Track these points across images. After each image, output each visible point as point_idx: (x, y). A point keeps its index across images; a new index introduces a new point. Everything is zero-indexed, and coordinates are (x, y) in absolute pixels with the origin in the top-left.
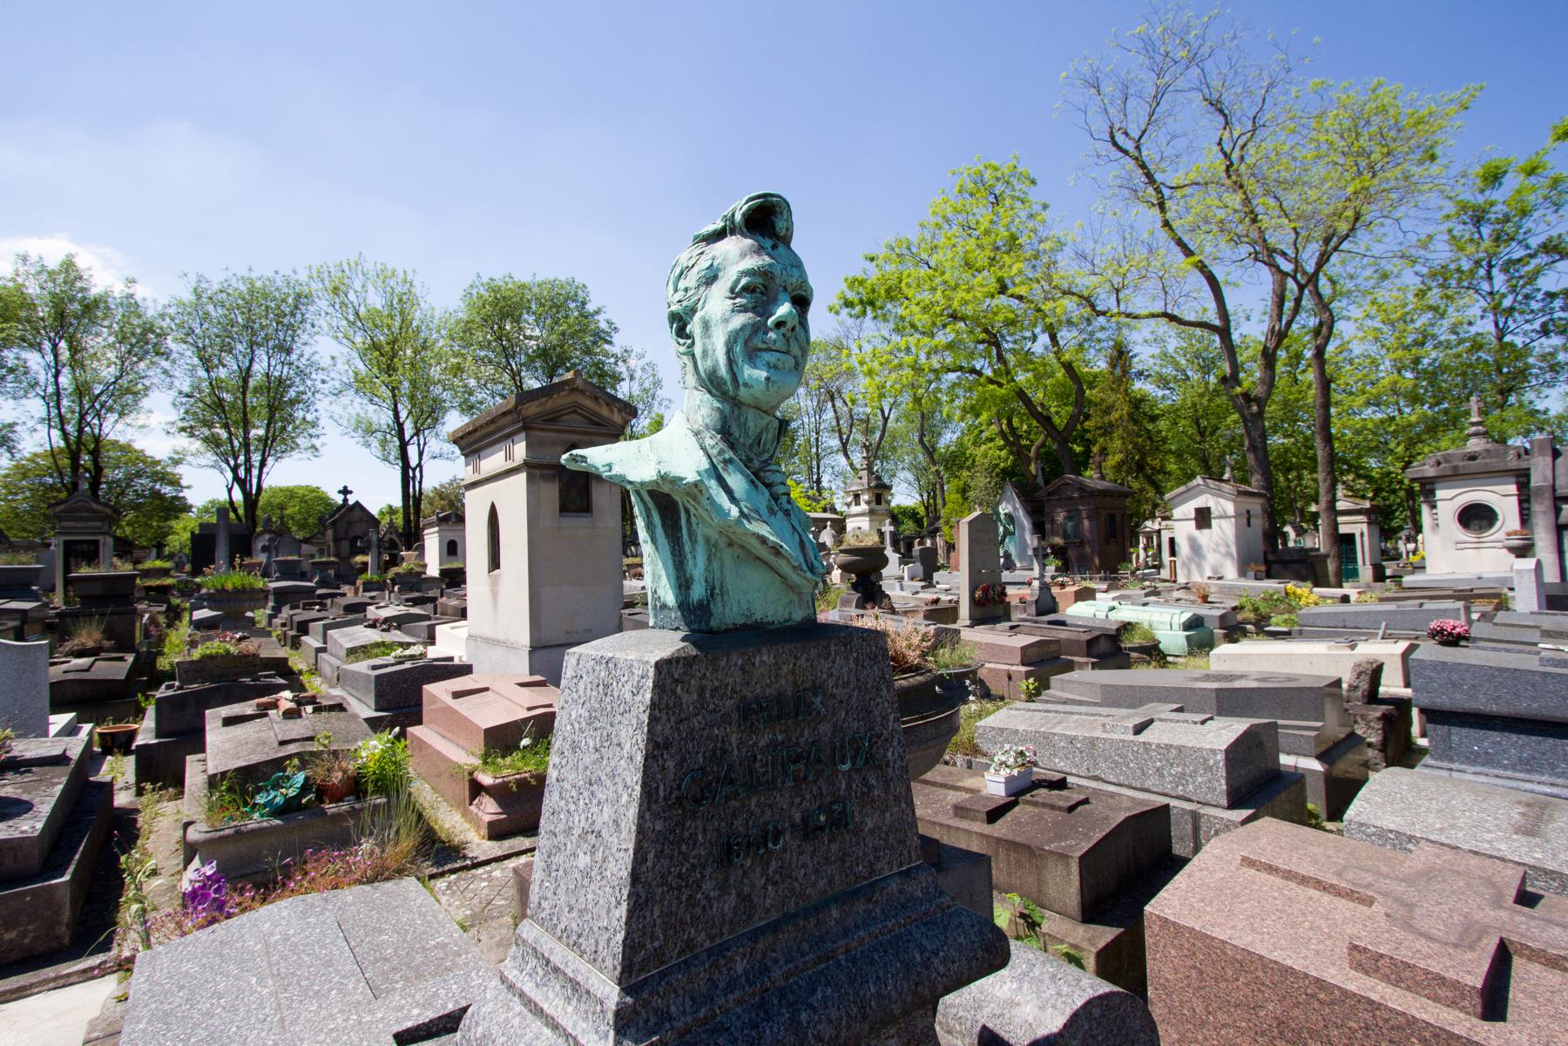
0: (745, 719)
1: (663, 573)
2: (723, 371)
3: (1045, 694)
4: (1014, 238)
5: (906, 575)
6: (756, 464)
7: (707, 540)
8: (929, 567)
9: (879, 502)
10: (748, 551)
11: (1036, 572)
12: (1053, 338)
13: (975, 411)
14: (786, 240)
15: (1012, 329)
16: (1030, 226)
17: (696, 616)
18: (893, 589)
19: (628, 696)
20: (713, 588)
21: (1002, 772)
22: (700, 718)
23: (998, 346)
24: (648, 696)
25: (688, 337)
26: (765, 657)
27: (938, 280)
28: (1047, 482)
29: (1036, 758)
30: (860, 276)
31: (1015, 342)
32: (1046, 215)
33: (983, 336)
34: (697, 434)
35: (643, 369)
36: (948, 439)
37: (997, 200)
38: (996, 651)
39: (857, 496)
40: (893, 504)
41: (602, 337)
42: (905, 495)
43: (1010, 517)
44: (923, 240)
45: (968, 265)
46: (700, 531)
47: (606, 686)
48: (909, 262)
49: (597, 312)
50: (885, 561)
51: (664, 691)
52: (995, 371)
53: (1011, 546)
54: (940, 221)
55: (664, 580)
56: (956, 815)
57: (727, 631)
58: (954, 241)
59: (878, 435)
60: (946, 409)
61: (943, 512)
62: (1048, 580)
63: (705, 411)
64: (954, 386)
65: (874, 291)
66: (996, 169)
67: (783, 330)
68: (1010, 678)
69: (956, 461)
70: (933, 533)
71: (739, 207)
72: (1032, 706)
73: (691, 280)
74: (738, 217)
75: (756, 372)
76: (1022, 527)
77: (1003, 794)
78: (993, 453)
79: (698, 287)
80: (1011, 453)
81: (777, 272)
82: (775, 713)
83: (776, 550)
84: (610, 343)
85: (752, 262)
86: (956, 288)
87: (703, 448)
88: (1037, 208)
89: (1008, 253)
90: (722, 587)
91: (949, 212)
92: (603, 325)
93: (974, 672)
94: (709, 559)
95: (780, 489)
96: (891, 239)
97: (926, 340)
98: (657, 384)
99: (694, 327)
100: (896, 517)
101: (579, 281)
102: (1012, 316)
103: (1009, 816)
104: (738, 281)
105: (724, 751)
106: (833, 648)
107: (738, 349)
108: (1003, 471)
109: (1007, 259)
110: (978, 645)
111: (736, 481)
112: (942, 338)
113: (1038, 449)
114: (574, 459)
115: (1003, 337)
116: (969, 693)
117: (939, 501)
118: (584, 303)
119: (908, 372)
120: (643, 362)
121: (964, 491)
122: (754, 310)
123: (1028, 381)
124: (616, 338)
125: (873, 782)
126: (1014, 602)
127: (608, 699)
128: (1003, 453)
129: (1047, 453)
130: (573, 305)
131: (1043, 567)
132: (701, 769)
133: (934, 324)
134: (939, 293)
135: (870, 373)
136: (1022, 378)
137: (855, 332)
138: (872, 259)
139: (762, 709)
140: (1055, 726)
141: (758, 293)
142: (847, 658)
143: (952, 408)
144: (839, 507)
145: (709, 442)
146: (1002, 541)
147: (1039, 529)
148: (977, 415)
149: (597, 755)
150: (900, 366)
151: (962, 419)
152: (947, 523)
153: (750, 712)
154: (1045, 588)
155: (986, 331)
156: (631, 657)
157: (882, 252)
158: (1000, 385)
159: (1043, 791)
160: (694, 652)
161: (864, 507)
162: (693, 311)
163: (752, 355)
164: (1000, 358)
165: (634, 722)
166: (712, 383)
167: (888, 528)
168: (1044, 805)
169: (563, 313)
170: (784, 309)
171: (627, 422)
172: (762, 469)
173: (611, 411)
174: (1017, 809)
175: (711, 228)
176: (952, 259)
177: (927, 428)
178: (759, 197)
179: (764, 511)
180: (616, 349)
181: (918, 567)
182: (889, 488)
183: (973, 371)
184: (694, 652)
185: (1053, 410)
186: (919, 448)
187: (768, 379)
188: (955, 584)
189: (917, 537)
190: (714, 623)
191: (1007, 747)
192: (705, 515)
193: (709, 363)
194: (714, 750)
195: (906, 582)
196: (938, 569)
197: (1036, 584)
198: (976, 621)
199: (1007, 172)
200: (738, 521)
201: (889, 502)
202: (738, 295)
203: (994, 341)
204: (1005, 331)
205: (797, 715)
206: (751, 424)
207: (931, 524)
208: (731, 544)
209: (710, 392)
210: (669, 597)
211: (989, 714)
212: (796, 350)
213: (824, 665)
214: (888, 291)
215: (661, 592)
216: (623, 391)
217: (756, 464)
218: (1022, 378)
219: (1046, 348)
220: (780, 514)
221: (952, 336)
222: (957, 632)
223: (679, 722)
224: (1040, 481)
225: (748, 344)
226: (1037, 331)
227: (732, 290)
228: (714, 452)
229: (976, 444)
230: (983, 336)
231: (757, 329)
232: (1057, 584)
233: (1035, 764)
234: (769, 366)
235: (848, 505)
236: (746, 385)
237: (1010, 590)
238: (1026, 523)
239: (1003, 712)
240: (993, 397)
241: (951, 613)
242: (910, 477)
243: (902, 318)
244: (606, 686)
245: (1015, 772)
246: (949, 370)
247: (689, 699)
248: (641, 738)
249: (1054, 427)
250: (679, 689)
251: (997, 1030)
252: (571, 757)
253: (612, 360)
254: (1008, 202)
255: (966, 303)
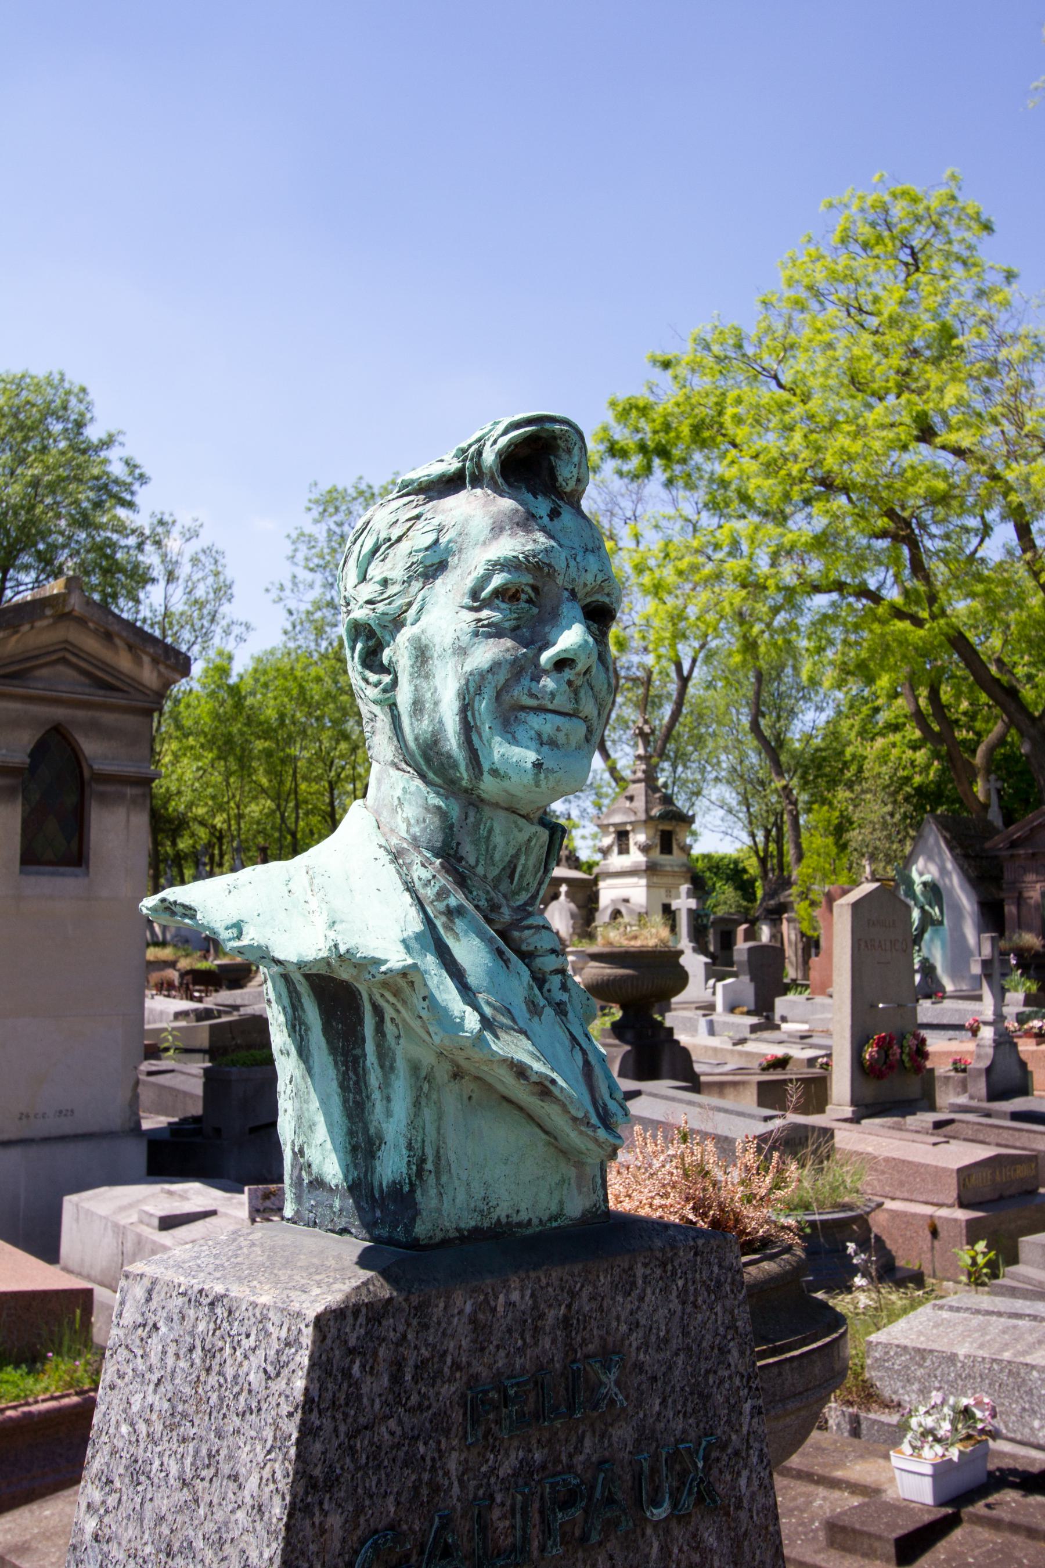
0: (475, 1422)
1: (320, 1119)
2: (452, 742)
3: (1010, 1274)
4: (947, 334)
5: (719, 1001)
6: (506, 915)
7: (415, 1068)
8: (767, 986)
9: (666, 847)
10: (488, 1087)
11: (987, 1008)
12: (1023, 531)
13: (865, 672)
14: (573, 500)
15: (941, 510)
16: (982, 312)
17: (383, 1211)
18: (693, 1030)
19: (255, 1378)
20: (423, 1160)
21: (927, 1452)
22: (392, 1423)
23: (914, 544)
24: (300, 1384)
25: (384, 669)
26: (515, 1295)
27: (798, 411)
28: (1009, 820)
29: (998, 1423)
30: (643, 396)
31: (947, 537)
32: (1008, 292)
33: (883, 523)
34: (396, 856)
35: (195, 561)
36: (808, 723)
37: (915, 263)
38: (907, 1176)
39: (622, 836)
40: (697, 850)
41: (113, 493)
42: (719, 834)
43: (934, 891)
44: (769, 330)
45: (856, 383)
46: (402, 1051)
47: (209, 1353)
48: (739, 372)
49: (107, 443)
50: (681, 979)
51: (329, 1373)
52: (906, 593)
53: (934, 950)
54: (803, 294)
55: (321, 1133)
56: (832, 1543)
57: (445, 1243)
58: (827, 337)
59: (667, 710)
60: (806, 669)
61: (796, 873)
62: (1012, 1024)
63: (412, 811)
64: (825, 619)
65: (667, 427)
66: (915, 200)
67: (568, 674)
68: (934, 1233)
69: (825, 768)
70: (776, 914)
71: (492, 429)
72: (984, 1300)
73: (394, 565)
74: (489, 457)
75: (517, 750)
76: (957, 909)
77: (929, 1499)
78: (897, 753)
79: (408, 581)
80: (936, 755)
81: (560, 564)
82: (530, 1407)
83: (544, 1089)
84: (130, 505)
85: (512, 545)
86: (833, 425)
87: (410, 888)
88: (992, 279)
89: (936, 361)
90: (438, 1157)
91: (820, 277)
92: (117, 469)
93: (862, 1220)
94: (417, 1104)
95: (550, 963)
96: (703, 327)
97: (771, 528)
98: (223, 591)
99: (398, 651)
100: (700, 879)
101: (75, 378)
102: (941, 485)
103: (941, 1550)
104: (486, 578)
105: (435, 1489)
106: (640, 1271)
107: (483, 705)
108: (919, 790)
109: (933, 376)
110: (870, 1162)
111: (470, 951)
112: (805, 525)
113: (991, 750)
114: (169, 908)
115: (923, 526)
116: (854, 1270)
117: (789, 847)
118: (80, 425)
119: (733, 595)
120: (194, 546)
121: (840, 830)
122: (514, 633)
123: (972, 614)
124: (142, 496)
125: (712, 1541)
126: (942, 1068)
127: (213, 1380)
128: (921, 756)
129: (1006, 758)
130: (57, 427)
131: (999, 994)
132: (391, 1527)
133: (787, 497)
134: (798, 437)
135: (657, 589)
136: (961, 607)
137: (627, 505)
138: (666, 365)
139: (506, 1400)
140: (1031, 1348)
141: (523, 603)
142: (665, 1290)
143: (818, 665)
144: (584, 855)
145: (419, 873)
146: (917, 940)
147: (992, 917)
148: (870, 680)
149: (186, 1495)
150: (718, 576)
151: (839, 685)
152: (804, 895)
153: (485, 1407)
154: (1005, 1042)
155: (891, 514)
156: (264, 1299)
157: (686, 352)
158: (918, 622)
159: (1010, 1496)
160: (385, 1291)
161: (636, 857)
162: (397, 623)
163: (509, 718)
164: (918, 568)
165: (268, 1433)
166: (428, 761)
167: (684, 903)
168: (1014, 1527)
169: (36, 442)
170: (571, 637)
171: (168, 684)
172: (516, 924)
173: (138, 662)
174: (957, 1534)
175: (436, 469)
176: (825, 373)
177: (767, 699)
178: (529, 422)
179: (520, 1010)
180: (141, 520)
181: (744, 985)
182: (687, 820)
183: (863, 592)
184: (385, 1291)
185: (1020, 671)
186: (751, 742)
187: (538, 765)
188: (821, 1022)
189: (741, 919)
190: (421, 1229)
191: (936, 1397)
192: (415, 1024)
193: (425, 725)
194: (416, 1488)
195: (720, 1014)
196: (785, 990)
197: (987, 1033)
198: (866, 1108)
199: (935, 205)
200: (479, 1038)
201: (686, 849)
202: (486, 604)
203: (904, 532)
204: (926, 516)
205: (571, 1408)
206: (498, 839)
207: (769, 895)
208: (457, 1075)
209: (423, 776)
210: (331, 1167)
211: (893, 1317)
212: (589, 708)
213: (622, 1305)
214: (697, 429)
215: (312, 1154)
216: (151, 604)
217: (506, 915)
218: (961, 607)
219: (1010, 552)
220: (549, 1012)
221: (820, 523)
222: (827, 1133)
223: (352, 1436)
224: (995, 816)
225: (503, 698)
226: (992, 516)
227: (474, 594)
228: (429, 893)
229: (866, 734)
230: (883, 523)
231: (523, 669)
232: (1028, 1034)
233: (995, 1435)
234: (541, 741)
235: (605, 852)
236: (495, 772)
237: (936, 1043)
238: (965, 901)
239: (925, 1313)
240: (902, 641)
241: (815, 1091)
242: (731, 797)
243: (724, 484)
244: (209, 1353)
245: (954, 1454)
246: (817, 589)
247: (375, 1386)
248: (282, 1468)
249: (1022, 707)
250: (356, 1369)
251: (18, 856)
252: (128, 1492)
253: (132, 541)
254: (936, 264)
255: (850, 458)
